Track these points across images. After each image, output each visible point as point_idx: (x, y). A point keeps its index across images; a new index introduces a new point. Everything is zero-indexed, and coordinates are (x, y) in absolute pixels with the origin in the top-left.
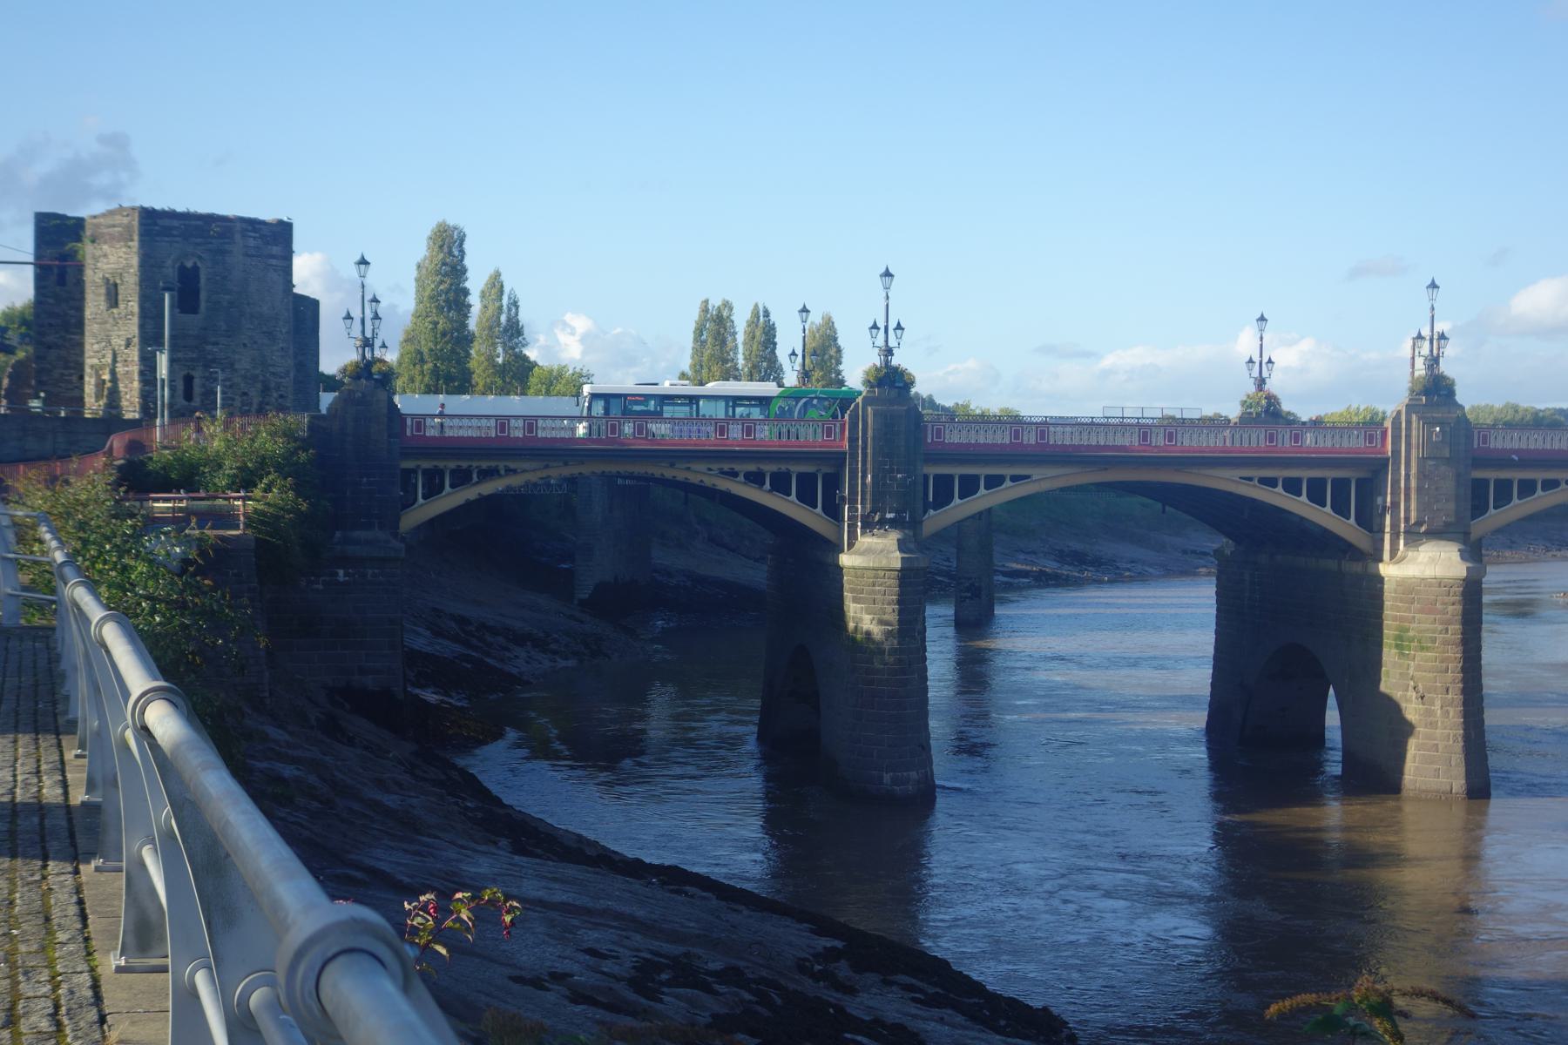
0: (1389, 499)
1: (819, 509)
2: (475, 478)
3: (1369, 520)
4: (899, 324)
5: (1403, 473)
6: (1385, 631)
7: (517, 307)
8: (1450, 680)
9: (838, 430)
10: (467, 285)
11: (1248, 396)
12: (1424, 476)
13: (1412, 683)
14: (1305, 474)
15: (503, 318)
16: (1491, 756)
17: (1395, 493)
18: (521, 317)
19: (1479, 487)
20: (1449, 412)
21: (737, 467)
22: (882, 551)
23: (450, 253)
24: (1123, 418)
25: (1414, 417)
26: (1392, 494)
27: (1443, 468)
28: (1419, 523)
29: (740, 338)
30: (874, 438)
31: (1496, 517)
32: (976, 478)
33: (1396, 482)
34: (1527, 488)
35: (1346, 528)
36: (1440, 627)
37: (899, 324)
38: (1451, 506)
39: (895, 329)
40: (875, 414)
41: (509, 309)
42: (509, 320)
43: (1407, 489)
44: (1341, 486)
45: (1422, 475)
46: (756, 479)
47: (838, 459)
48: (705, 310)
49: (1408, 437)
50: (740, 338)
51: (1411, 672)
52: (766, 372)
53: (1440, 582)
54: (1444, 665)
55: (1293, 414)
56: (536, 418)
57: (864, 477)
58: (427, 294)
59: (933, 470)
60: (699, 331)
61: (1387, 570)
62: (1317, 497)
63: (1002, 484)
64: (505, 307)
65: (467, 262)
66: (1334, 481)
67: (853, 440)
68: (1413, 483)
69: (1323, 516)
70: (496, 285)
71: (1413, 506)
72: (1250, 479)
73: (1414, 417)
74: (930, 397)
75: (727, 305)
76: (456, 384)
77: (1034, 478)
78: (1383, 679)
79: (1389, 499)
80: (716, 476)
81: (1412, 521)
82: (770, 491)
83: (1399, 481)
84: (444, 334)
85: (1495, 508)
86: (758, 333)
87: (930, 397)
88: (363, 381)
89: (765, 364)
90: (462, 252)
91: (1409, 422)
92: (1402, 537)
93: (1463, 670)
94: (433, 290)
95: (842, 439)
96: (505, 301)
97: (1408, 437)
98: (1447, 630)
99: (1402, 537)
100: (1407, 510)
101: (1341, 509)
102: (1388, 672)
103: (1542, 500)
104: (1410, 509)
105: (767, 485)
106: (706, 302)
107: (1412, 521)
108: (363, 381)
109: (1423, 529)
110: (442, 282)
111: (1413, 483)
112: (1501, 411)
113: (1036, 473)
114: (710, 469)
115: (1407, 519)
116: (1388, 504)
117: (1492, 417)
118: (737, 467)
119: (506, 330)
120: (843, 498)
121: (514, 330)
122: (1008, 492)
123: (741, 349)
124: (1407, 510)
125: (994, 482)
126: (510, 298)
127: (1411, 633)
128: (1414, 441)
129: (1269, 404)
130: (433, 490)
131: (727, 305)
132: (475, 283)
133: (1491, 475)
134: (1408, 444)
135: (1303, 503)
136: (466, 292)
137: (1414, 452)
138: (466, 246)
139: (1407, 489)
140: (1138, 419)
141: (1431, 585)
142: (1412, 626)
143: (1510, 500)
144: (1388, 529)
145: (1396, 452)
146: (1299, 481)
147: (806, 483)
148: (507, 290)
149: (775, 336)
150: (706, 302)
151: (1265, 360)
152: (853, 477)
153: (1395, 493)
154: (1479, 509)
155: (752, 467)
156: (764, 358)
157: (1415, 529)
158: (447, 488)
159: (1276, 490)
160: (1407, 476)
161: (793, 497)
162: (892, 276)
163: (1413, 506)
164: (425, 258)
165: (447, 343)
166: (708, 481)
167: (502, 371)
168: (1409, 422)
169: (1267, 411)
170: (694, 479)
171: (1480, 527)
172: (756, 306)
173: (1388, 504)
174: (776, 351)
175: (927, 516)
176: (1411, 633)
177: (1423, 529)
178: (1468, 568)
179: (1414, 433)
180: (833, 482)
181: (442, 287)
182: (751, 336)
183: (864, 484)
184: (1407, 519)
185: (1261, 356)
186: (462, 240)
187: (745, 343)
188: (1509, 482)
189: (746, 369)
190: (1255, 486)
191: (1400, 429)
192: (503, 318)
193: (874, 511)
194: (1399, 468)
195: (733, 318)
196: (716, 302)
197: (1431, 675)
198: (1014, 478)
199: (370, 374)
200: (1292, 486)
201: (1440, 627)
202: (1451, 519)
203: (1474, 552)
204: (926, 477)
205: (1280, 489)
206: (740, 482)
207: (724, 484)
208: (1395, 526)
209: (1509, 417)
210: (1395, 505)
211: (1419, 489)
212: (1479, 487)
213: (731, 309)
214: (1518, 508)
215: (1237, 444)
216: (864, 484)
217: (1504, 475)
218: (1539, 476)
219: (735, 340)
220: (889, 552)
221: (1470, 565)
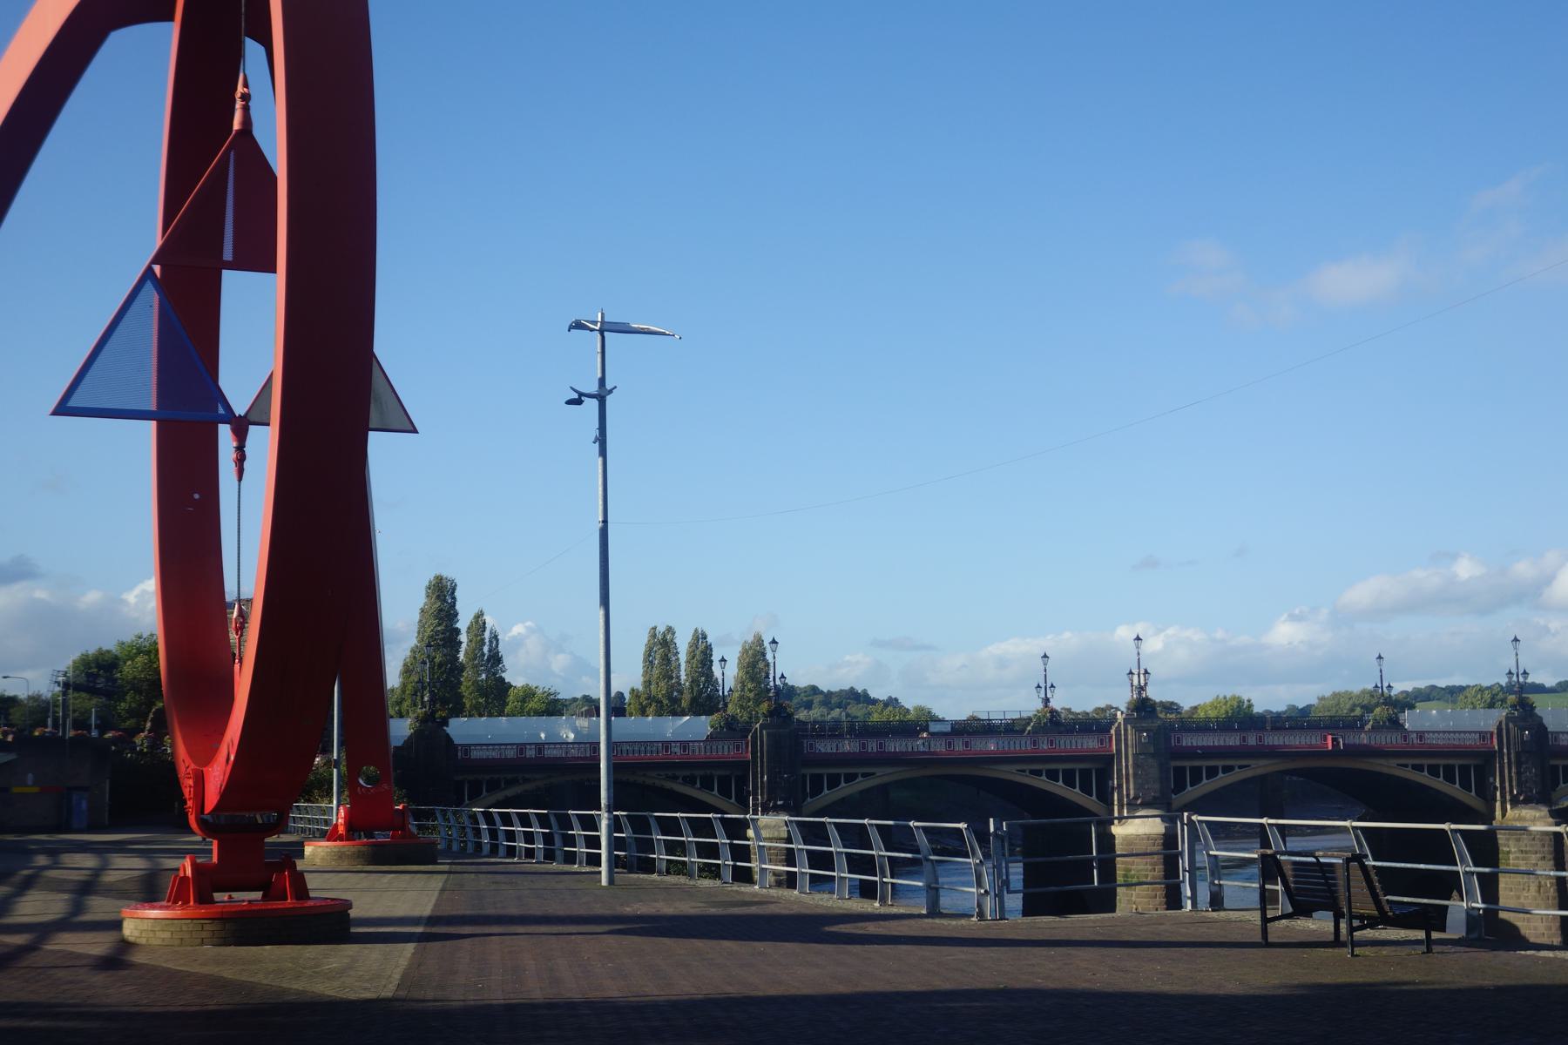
0: (1115, 782)
1: (733, 800)
2: (503, 785)
3: (1105, 797)
4: (782, 675)
5: (1124, 764)
6: (1118, 872)
7: (497, 641)
8: (1157, 903)
9: (744, 747)
10: (458, 625)
11: (1038, 711)
12: (1138, 766)
13: (1134, 906)
14: (1061, 766)
15: (486, 649)
16: (1017, 898)
17: (1120, 778)
18: (500, 648)
19: (1180, 772)
20: (1153, 723)
21: (678, 773)
22: (775, 826)
23: (445, 601)
24: (989, 720)
25: (1129, 727)
26: (1117, 779)
27: (1150, 760)
28: (1136, 798)
29: (683, 657)
30: (768, 752)
31: (1192, 792)
32: (839, 775)
33: (1119, 771)
34: (1212, 772)
35: (1091, 802)
36: (1150, 867)
37: (782, 675)
38: (1157, 786)
39: (780, 678)
40: (768, 734)
41: (491, 642)
42: (490, 651)
43: (1127, 775)
44: (1085, 774)
45: (1136, 765)
46: (690, 781)
47: (744, 766)
48: (654, 636)
49: (1126, 740)
50: (683, 657)
51: (1133, 899)
52: (704, 685)
53: (1148, 837)
54: (1154, 893)
55: (1176, 704)
56: (1423, 732)
57: (762, 777)
58: (427, 635)
59: (808, 771)
60: (649, 653)
61: (1117, 830)
62: (1450, 778)
63: (855, 779)
64: (487, 641)
65: (458, 607)
66: (1081, 770)
67: (754, 753)
68: (1131, 771)
69: (1075, 795)
70: (479, 624)
71: (1131, 786)
72: (1024, 771)
73: (1129, 727)
74: (865, 691)
75: (670, 630)
76: (451, 706)
77: (1253, 766)
78: (1118, 904)
79: (1115, 782)
80: (664, 779)
81: (1132, 797)
82: (700, 789)
83: (1122, 770)
84: (440, 665)
85: (1191, 786)
86: (698, 652)
87: (865, 691)
88: (430, 724)
89: (703, 678)
90: (454, 599)
91: (1126, 730)
92: (1125, 807)
93: (1167, 896)
94: (432, 630)
95: (747, 752)
96: (487, 635)
97: (1126, 740)
98: (1155, 869)
99: (1125, 807)
100: (1128, 789)
101: (1086, 789)
102: (1120, 900)
103: (1222, 780)
104: (1130, 789)
105: (698, 785)
106: (655, 628)
107: (1132, 797)
108: (430, 724)
109: (1139, 802)
110: (440, 625)
111: (1131, 771)
112: (1358, 697)
113: (879, 771)
114: (659, 775)
115: (1128, 795)
116: (1116, 785)
117: (1351, 702)
118: (678, 773)
119: (489, 660)
120: (1113, 788)
121: (496, 659)
122: (1237, 776)
123: (683, 667)
124: (1128, 789)
125: (850, 778)
126: (491, 633)
127: (1133, 872)
128: (1130, 743)
129: (1052, 716)
130: (1196, 780)
131: (670, 630)
132: (463, 623)
133: (1187, 764)
134: (1126, 745)
135: (1060, 786)
136: (458, 631)
137: (1130, 749)
138: (457, 594)
139: (1127, 775)
140: (1001, 720)
141: (1143, 839)
142: (1133, 867)
143: (1201, 780)
144: (1116, 803)
145: (1119, 750)
146: (1057, 771)
147: (1465, 770)
148: (488, 626)
149: (711, 655)
150: (655, 628)
151: (1049, 685)
152: (755, 778)
153: (1120, 778)
154: (1180, 787)
155: (687, 773)
156: (702, 674)
157: (1133, 802)
158: (484, 793)
159: (1041, 778)
160: (1127, 766)
161: (715, 792)
162: (777, 643)
163: (1131, 786)
164: (425, 604)
165: (442, 673)
166: (658, 783)
167: (482, 690)
168: (1126, 730)
169: (1051, 720)
170: (649, 782)
171: (1178, 799)
172: (696, 630)
173: (1116, 785)
174: (713, 668)
175: (805, 803)
176: (1133, 872)
177: (1139, 802)
178: (1166, 827)
179: (1129, 737)
180: (742, 781)
181: (439, 628)
182: (692, 655)
183: (762, 782)
184: (1128, 795)
185: (1046, 683)
186: (454, 589)
187: (688, 662)
188: (1200, 768)
189: (687, 684)
190: (1027, 776)
191: (1121, 734)
192: (486, 649)
193: (769, 800)
194: (1121, 762)
195: (676, 641)
196: (661, 629)
197: (1146, 900)
198: (864, 775)
199: (435, 719)
200: (1052, 775)
201: (1150, 867)
202: (1157, 795)
203: (1170, 820)
204: (804, 776)
205: (1044, 778)
206: (680, 783)
207: (669, 785)
208: (1121, 800)
209: (1366, 702)
210: (1120, 786)
211: (1135, 775)
212: (1180, 772)
213: (674, 633)
214: (1207, 786)
215: (1012, 748)
216: (762, 782)
217: (1197, 763)
218: (1220, 763)
219: (678, 659)
220: (779, 827)
221: (1167, 825)
